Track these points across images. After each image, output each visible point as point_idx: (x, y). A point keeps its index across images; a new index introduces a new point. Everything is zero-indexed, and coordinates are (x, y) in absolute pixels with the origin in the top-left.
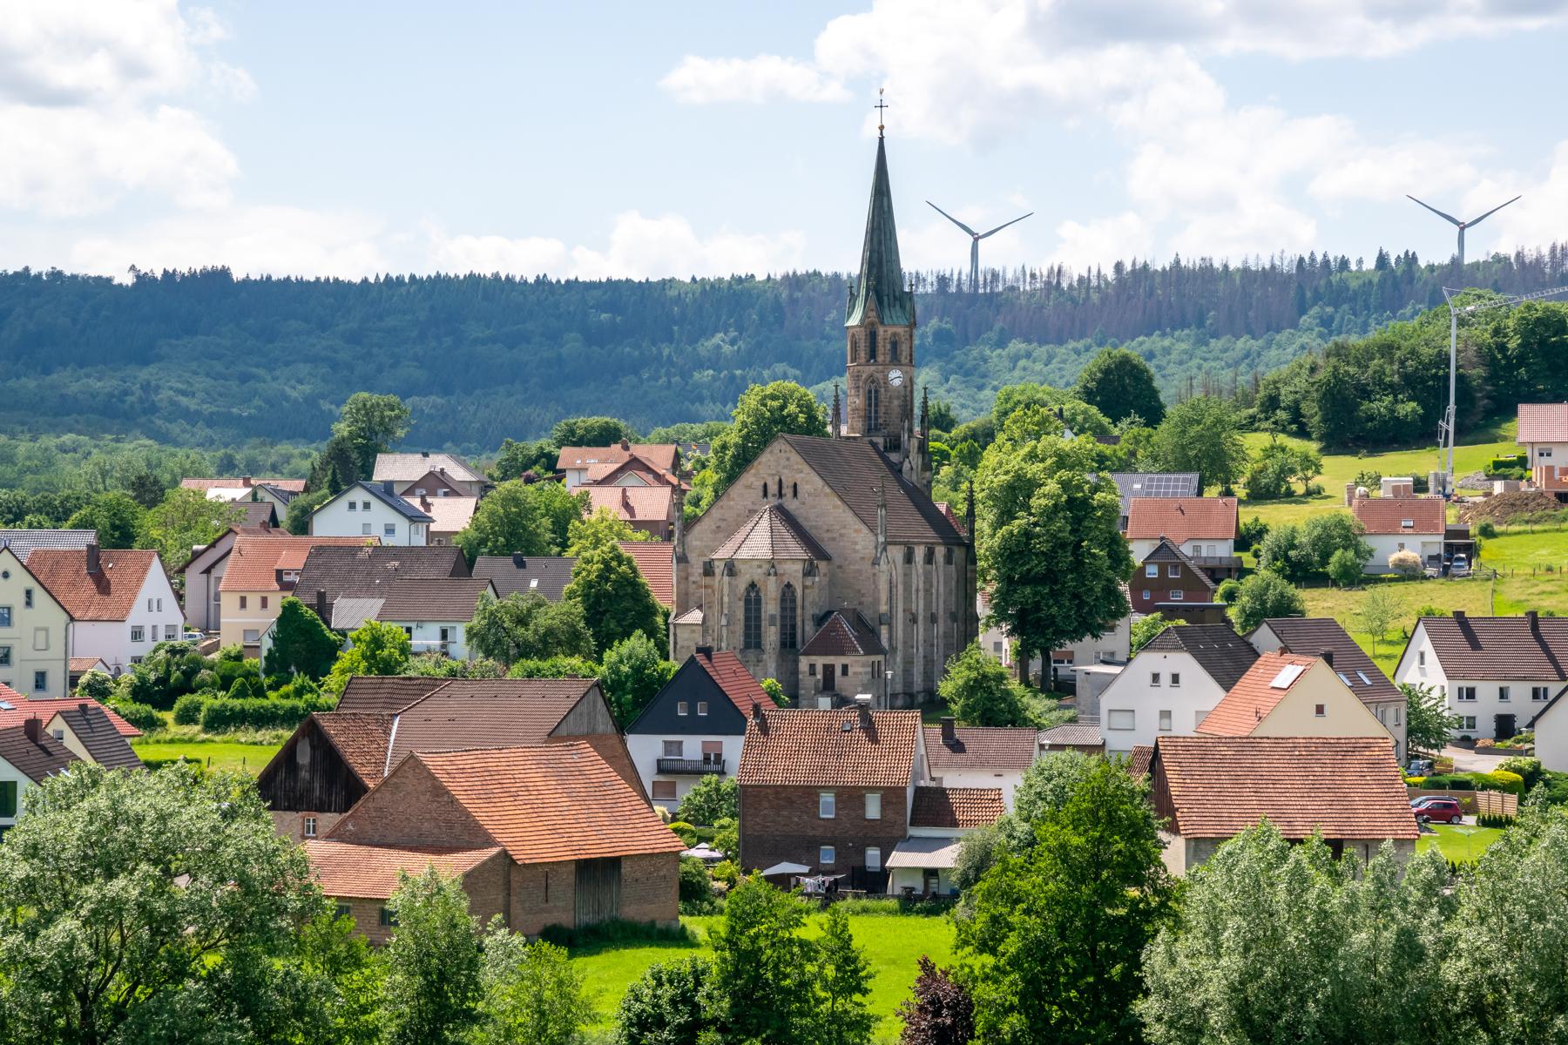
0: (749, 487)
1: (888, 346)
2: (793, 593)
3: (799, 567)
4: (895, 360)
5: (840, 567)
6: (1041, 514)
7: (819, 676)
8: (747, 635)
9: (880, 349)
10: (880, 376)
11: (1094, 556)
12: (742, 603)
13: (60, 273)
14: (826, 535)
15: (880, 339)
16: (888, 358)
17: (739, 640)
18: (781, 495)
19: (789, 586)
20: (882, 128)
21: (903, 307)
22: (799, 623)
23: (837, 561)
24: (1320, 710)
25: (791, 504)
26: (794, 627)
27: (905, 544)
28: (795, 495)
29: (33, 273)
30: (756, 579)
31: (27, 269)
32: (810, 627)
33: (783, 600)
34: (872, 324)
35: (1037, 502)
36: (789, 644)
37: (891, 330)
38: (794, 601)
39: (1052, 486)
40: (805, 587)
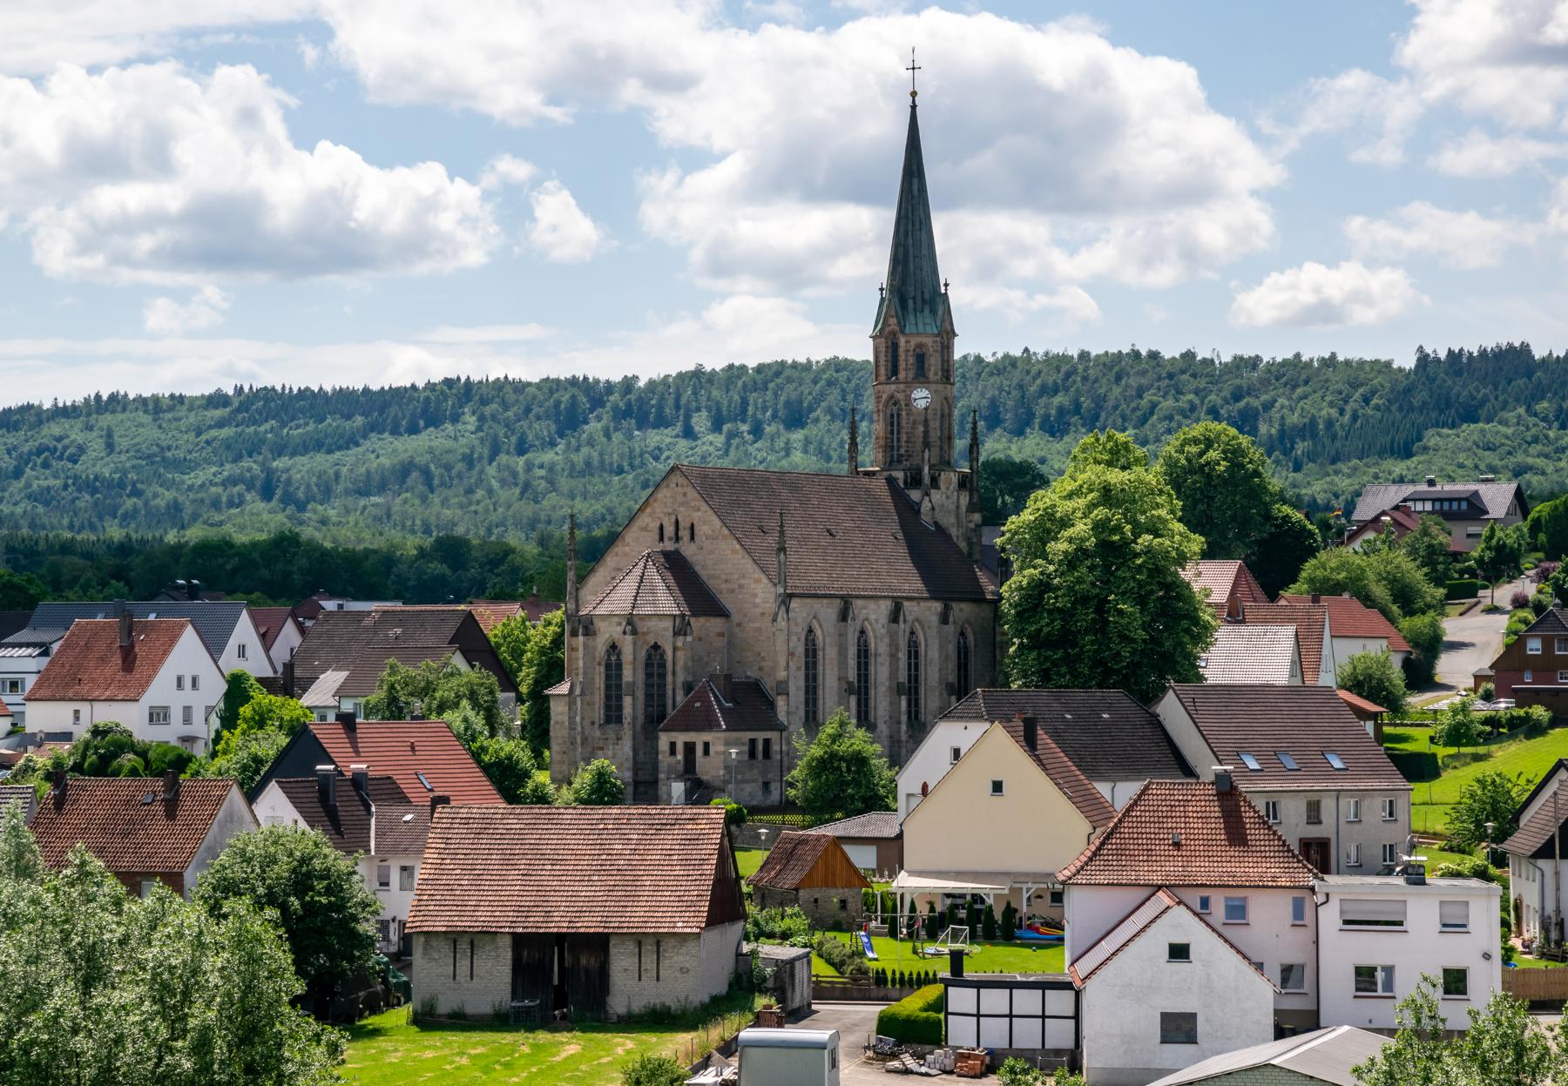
0: (645, 529)
1: (911, 360)
2: (662, 656)
3: (668, 624)
4: (921, 376)
5: (739, 625)
6: (1060, 563)
7: (680, 757)
8: (608, 708)
9: (902, 365)
10: (900, 396)
11: (1121, 612)
12: (602, 669)
13: (1241, 358)
14: (724, 586)
15: (901, 350)
16: (911, 375)
17: (598, 712)
18: (677, 539)
19: (656, 647)
20: (914, 94)
21: (933, 312)
22: (670, 693)
23: (735, 618)
24: (997, 787)
25: (688, 550)
26: (663, 696)
27: (841, 597)
28: (692, 538)
29: (1305, 358)
30: (616, 637)
31: (1298, 356)
32: (680, 698)
33: (648, 664)
34: (894, 334)
35: (1059, 547)
36: (655, 719)
37: (914, 341)
38: (663, 665)
39: (1081, 528)
40: (675, 649)
